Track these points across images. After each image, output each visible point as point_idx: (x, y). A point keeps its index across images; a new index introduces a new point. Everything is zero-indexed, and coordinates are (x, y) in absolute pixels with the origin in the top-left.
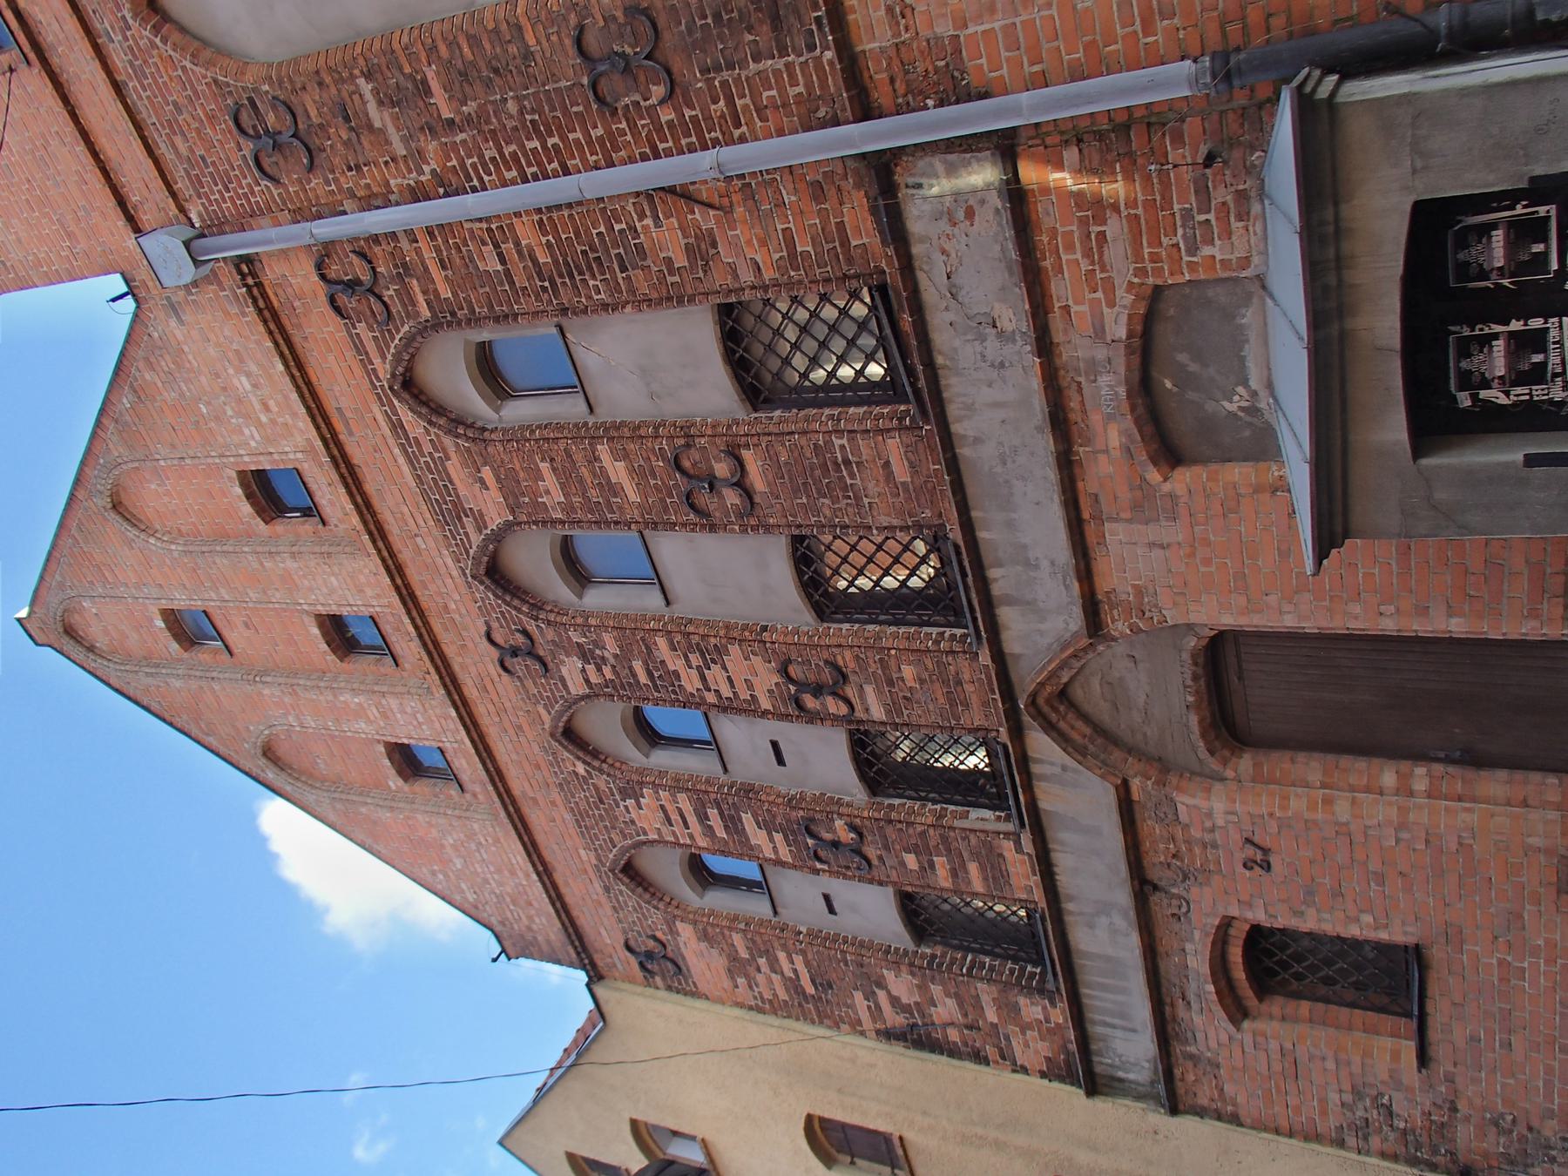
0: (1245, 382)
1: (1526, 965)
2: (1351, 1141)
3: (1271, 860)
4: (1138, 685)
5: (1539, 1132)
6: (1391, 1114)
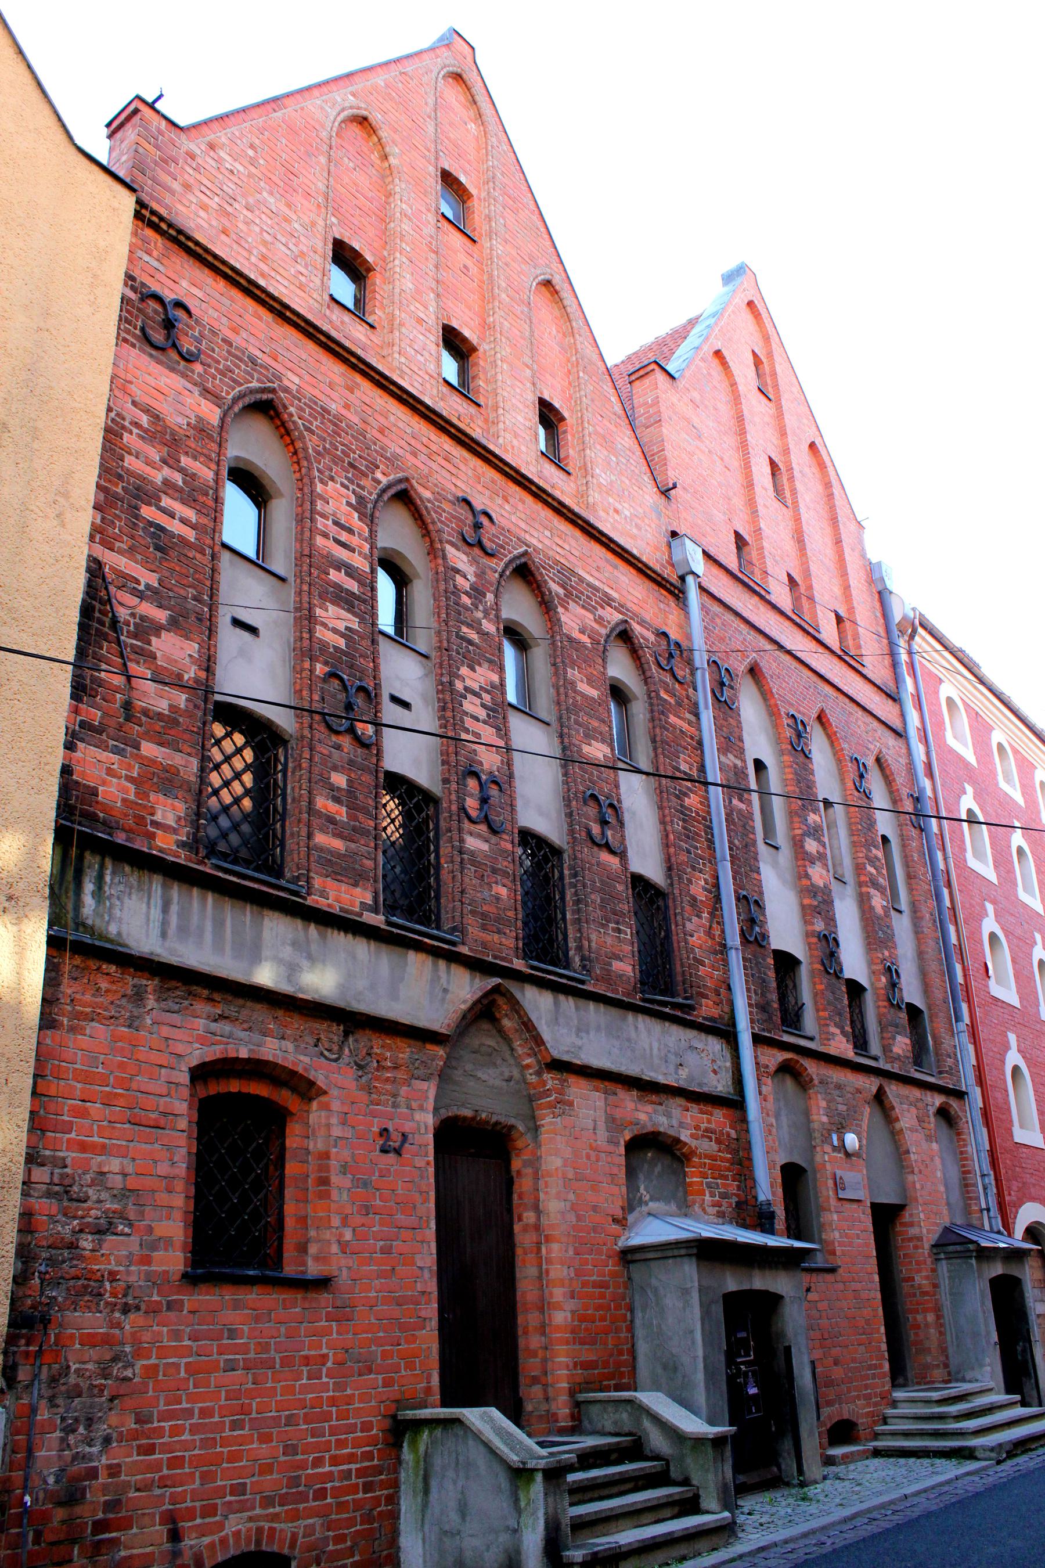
0: (652, 1199)
1: (325, 1380)
3: (391, 1155)
4: (491, 1076)
5: (110, 1409)
6: (99, 1232)
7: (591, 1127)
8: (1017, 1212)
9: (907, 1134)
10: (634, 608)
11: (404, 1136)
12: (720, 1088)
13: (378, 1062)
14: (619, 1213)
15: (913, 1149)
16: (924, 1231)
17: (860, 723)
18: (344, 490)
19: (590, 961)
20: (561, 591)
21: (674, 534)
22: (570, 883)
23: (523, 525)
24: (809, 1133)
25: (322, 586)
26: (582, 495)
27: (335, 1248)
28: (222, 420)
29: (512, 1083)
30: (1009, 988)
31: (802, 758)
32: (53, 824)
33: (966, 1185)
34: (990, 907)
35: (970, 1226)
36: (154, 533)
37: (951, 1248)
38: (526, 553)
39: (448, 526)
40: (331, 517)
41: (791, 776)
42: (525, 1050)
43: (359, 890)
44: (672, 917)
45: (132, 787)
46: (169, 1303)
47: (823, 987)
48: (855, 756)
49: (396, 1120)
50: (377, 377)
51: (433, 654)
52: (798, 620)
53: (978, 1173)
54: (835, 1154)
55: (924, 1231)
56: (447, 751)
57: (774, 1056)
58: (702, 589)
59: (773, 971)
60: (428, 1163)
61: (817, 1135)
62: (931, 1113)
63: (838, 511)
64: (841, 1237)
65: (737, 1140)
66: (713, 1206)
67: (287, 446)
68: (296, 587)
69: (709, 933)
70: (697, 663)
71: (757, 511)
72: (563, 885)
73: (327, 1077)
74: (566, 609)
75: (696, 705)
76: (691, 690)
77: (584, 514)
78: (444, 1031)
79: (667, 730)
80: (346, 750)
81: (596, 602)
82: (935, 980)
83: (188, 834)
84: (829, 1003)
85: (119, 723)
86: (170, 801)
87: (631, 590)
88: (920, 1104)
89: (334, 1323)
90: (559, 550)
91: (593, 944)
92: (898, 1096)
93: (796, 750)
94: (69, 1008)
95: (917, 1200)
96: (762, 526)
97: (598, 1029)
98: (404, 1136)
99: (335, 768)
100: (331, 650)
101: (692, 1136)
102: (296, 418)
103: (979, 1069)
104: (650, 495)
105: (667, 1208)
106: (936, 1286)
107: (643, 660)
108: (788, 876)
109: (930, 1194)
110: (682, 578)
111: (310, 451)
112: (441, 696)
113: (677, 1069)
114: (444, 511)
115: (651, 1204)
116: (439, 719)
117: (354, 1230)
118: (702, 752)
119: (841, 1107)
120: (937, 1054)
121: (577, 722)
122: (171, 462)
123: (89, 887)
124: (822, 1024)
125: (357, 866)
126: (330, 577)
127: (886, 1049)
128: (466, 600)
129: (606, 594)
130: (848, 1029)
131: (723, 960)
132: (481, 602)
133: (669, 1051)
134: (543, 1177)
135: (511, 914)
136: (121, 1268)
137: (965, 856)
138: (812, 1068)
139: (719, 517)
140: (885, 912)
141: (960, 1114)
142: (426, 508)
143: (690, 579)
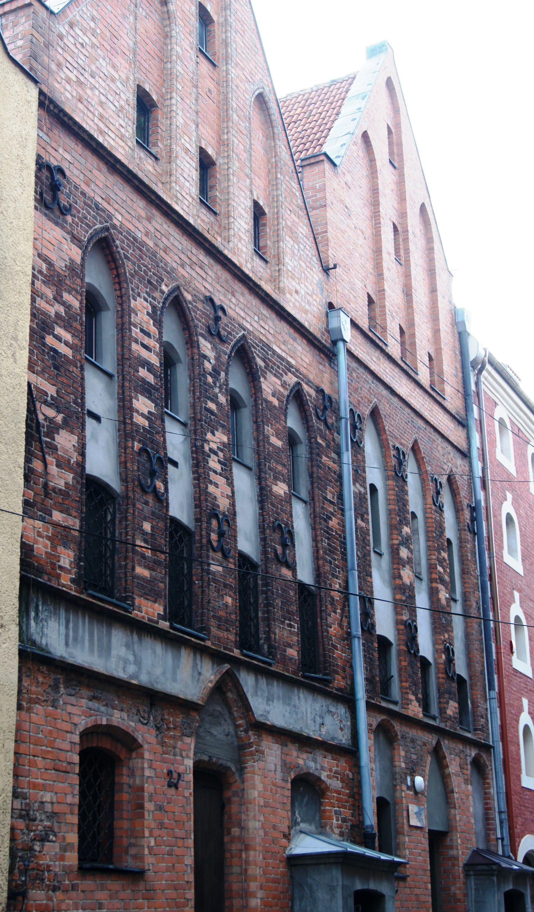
2: (18, 804)
7: (273, 769)
8: (520, 842)
9: (453, 778)
10: (305, 371)
11: (179, 775)
12: (344, 741)
13: (167, 724)
14: (286, 830)
15: (456, 790)
16: (460, 853)
17: (439, 448)
18: (145, 303)
19: (275, 649)
20: (262, 364)
21: (331, 306)
22: (262, 590)
23: (242, 314)
24: (393, 776)
25: (135, 381)
26: (275, 280)
27: (146, 852)
28: (83, 259)
29: (229, 737)
30: (525, 661)
31: (401, 483)
32: (19, 575)
33: (487, 819)
34: (517, 595)
35: (488, 851)
36: (53, 356)
37: (479, 867)
38: (244, 336)
39: (200, 321)
40: (139, 326)
41: (393, 497)
42: (239, 714)
43: (157, 605)
44: (319, 613)
45: (49, 543)
46: (73, 885)
47: (406, 664)
48: (436, 476)
49: (175, 765)
50: (166, 209)
51: (189, 422)
52: (405, 367)
53: (497, 810)
54: (408, 792)
55: (460, 853)
56: (200, 497)
57: (375, 717)
58: (349, 353)
59: (377, 652)
60: (190, 794)
61: (398, 776)
62: (468, 761)
63: (436, 263)
64: (410, 854)
65: (352, 779)
66: (338, 827)
67: (111, 269)
68: (118, 382)
69: (340, 625)
70: (343, 414)
71: (382, 274)
72: (257, 592)
73: (143, 736)
74: (265, 378)
75: (338, 446)
76: (335, 434)
77: (274, 296)
78: (195, 699)
79: (320, 468)
80: (150, 505)
81: (283, 370)
82: (476, 655)
83: (76, 573)
84: (410, 676)
85: (42, 499)
86: (66, 551)
87: (303, 357)
88: (462, 755)
89: (146, 901)
90: (262, 331)
91: (277, 637)
92: (449, 748)
93: (397, 476)
94: (26, 696)
95: (457, 830)
96: (386, 288)
97: (278, 698)
98: (179, 775)
99: (145, 519)
100: (142, 431)
101: (328, 776)
102: (119, 249)
103: (503, 727)
104: (317, 274)
105: (310, 827)
106: (466, 895)
107: (308, 413)
108: (387, 577)
109: (465, 825)
110: (334, 343)
111: (128, 274)
112: (194, 455)
113: (320, 727)
114: (198, 310)
115: (301, 825)
116: (194, 473)
117: (155, 839)
118: (341, 485)
119: (414, 757)
120: (474, 716)
121: (270, 468)
122: (59, 299)
123: (33, 614)
124: (404, 693)
125: (156, 588)
126: (140, 374)
127: (442, 711)
128: (210, 379)
129: (288, 363)
130: (420, 696)
131: (348, 645)
132: (218, 380)
133: (316, 714)
134: (244, 804)
135: (233, 616)
136: (52, 863)
137: (502, 553)
138: (398, 727)
139: (359, 284)
140: (447, 602)
141: (487, 763)
142: (188, 308)
143: (341, 345)
